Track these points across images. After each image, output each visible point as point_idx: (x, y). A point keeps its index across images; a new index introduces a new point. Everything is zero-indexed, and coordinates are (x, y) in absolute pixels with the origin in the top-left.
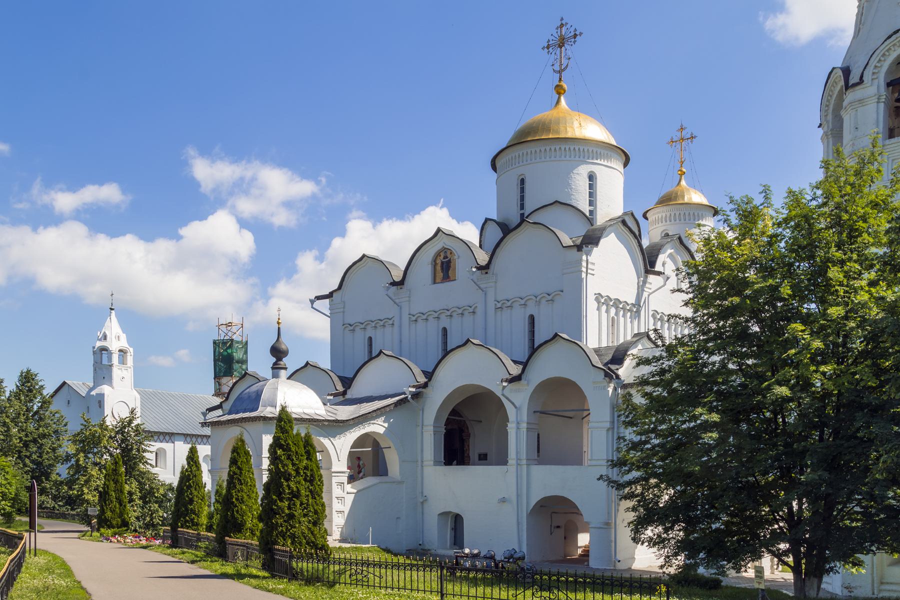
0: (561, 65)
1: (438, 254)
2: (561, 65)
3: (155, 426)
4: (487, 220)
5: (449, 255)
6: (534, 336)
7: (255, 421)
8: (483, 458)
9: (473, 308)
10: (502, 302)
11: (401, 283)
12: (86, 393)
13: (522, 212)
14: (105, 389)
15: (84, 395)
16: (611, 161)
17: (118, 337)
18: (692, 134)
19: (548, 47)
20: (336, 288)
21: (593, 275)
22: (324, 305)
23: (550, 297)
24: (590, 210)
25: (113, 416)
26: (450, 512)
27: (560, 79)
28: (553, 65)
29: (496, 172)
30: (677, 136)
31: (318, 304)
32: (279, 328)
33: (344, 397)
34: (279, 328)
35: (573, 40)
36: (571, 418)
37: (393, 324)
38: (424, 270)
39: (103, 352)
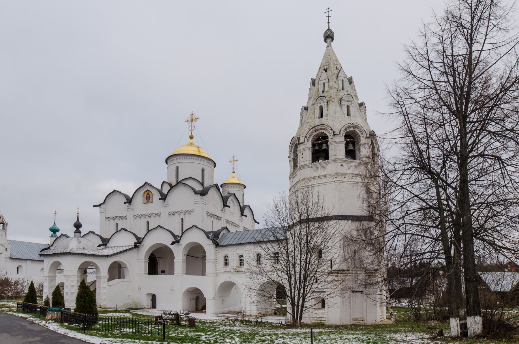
0: (192, 128)
2: (192, 128)
6: (183, 223)
8: (163, 272)
13: (177, 180)
23: (190, 212)
26: (151, 293)
27: (192, 133)
29: (167, 164)
32: (78, 216)
34: (78, 216)
36: (197, 258)
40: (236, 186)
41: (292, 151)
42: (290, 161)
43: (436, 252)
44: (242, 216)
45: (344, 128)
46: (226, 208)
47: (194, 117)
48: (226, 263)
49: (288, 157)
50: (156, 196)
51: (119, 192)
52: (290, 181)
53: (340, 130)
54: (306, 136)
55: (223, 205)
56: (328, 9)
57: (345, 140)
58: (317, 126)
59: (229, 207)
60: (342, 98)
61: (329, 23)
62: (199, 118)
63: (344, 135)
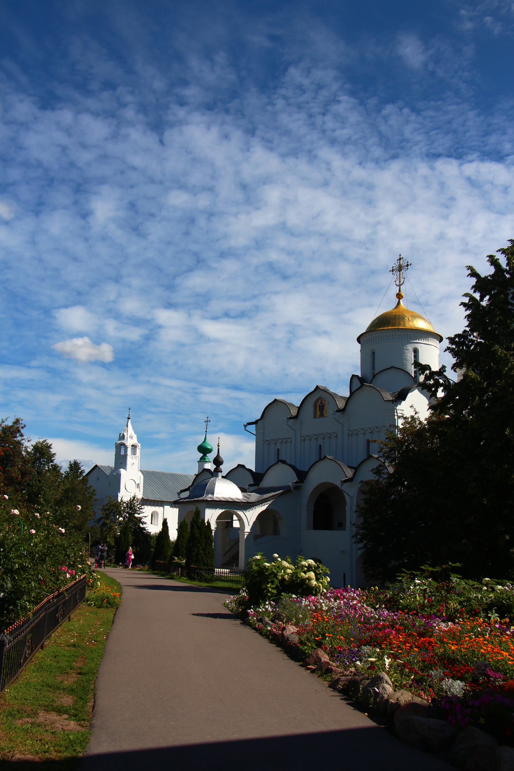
0: (400, 282)
1: (317, 401)
2: (400, 282)
3: (152, 496)
4: (353, 376)
5: (323, 402)
7: (202, 502)
9: (336, 434)
10: (352, 431)
11: (296, 417)
12: (109, 473)
13: (373, 371)
14: (122, 471)
15: (108, 475)
16: (428, 339)
17: (132, 436)
19: (393, 271)
20: (259, 417)
22: (252, 428)
24: (414, 371)
25: (126, 489)
27: (400, 291)
28: (395, 281)
31: (249, 427)
33: (258, 487)
34: (218, 449)
35: (406, 268)
37: (291, 442)
38: (309, 409)
39: (121, 446)
40: (406, 334)
47: (403, 263)
62: (411, 264)
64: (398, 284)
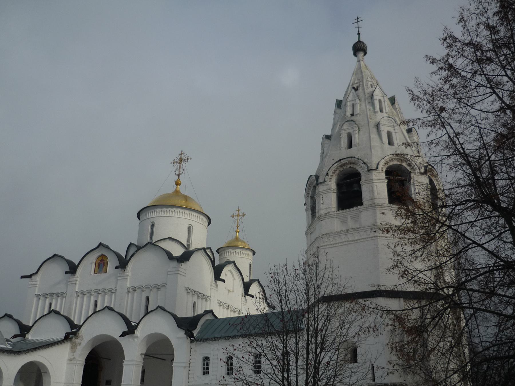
2: (179, 172)
6: (148, 304)
18: (243, 213)
19: (174, 163)
21: (185, 276)
23: (158, 288)
27: (179, 178)
29: (139, 220)
30: (236, 213)
35: (186, 161)
36: (165, 360)
41: (310, 196)
42: (306, 210)
43: (316, 327)
44: (247, 296)
45: (383, 161)
46: (219, 282)
48: (206, 370)
49: (305, 205)
50: (112, 263)
51: (62, 257)
52: (307, 239)
53: (378, 164)
54: (327, 174)
55: (214, 278)
56: (358, 19)
57: (386, 178)
58: (343, 159)
59: (224, 281)
60: (380, 122)
61: (359, 34)
63: (384, 170)
64: (177, 173)
